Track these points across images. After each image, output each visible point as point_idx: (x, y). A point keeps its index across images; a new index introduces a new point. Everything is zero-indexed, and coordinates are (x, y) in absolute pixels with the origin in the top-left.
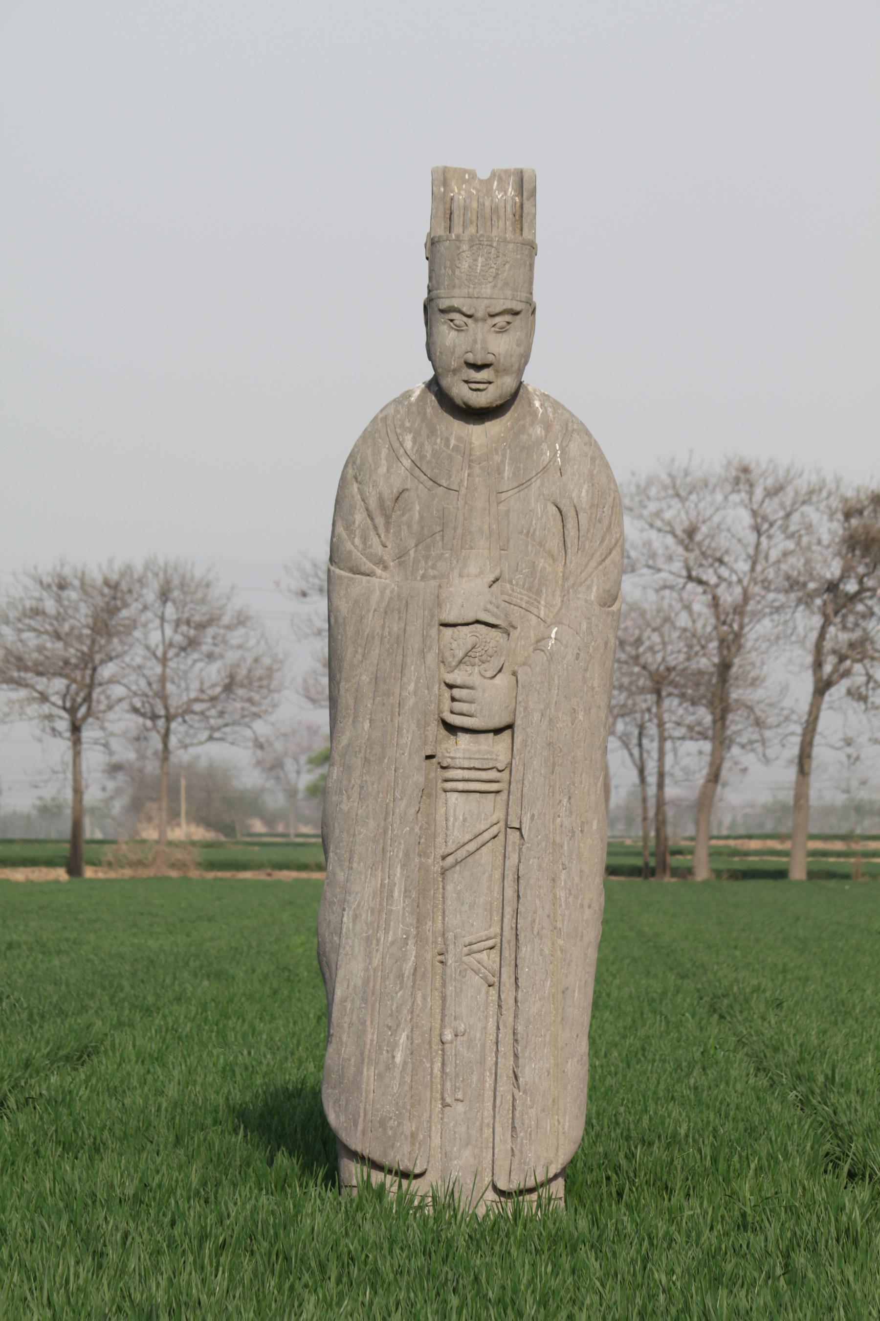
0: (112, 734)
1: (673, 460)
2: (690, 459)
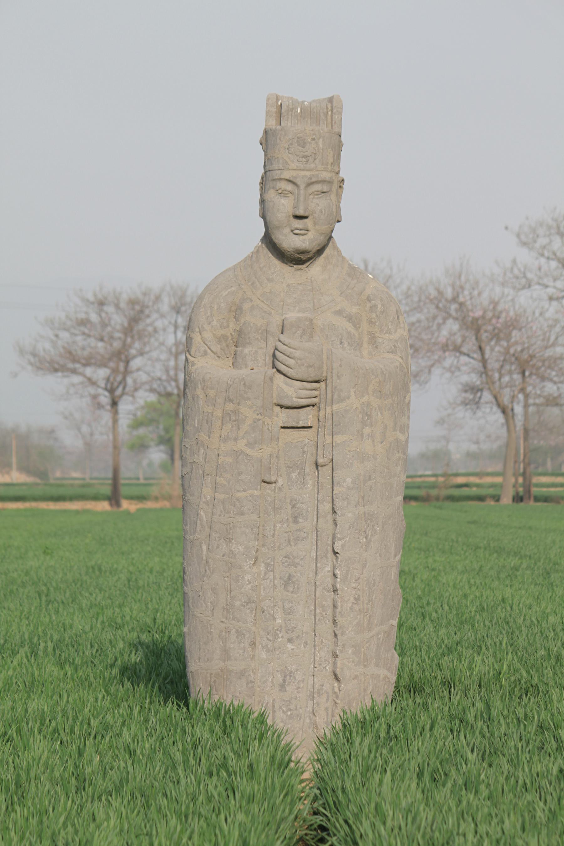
1: (555, 209)
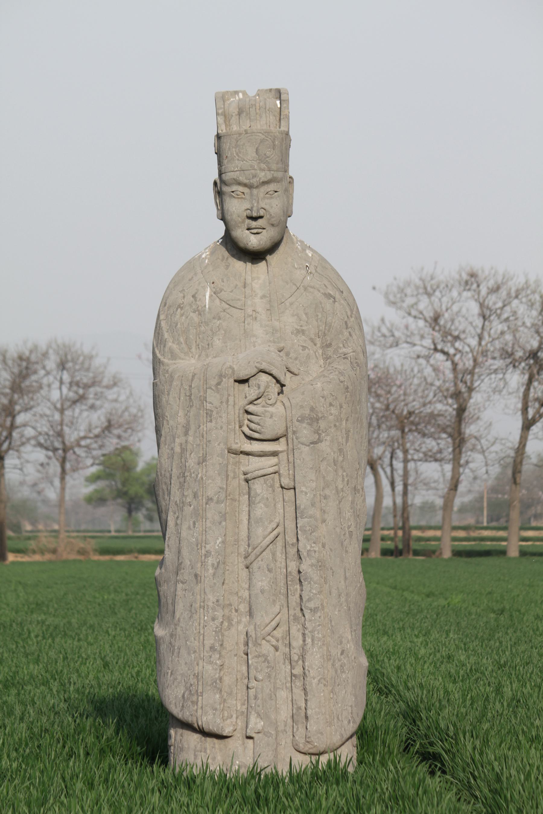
0: (28, 462)
1: (422, 269)
2: (435, 268)
